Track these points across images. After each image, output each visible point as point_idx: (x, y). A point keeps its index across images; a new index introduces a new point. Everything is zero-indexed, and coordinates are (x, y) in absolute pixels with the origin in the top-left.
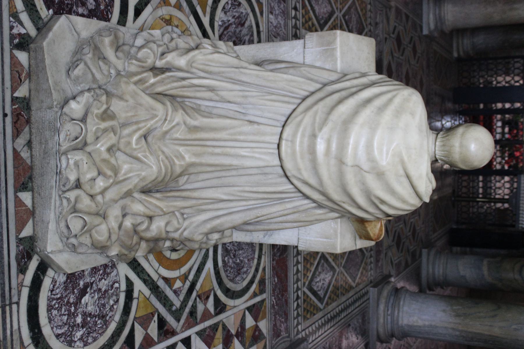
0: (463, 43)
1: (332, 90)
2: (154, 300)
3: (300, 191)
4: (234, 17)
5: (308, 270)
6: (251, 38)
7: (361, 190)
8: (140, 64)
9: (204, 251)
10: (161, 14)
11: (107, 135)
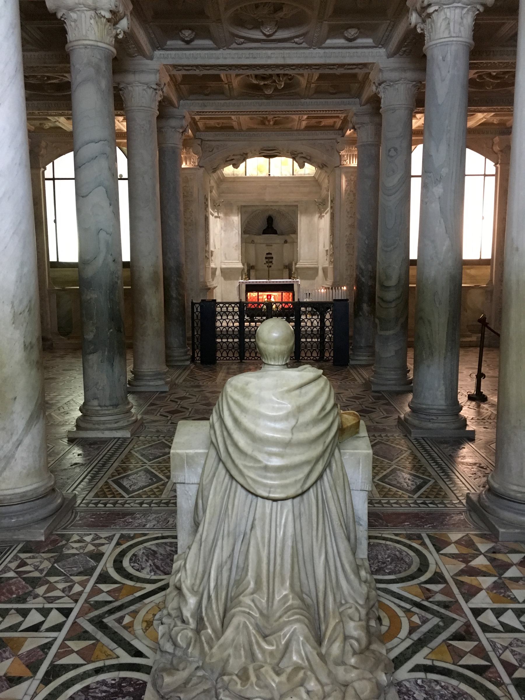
0: (178, 357)
1: (223, 456)
2: (434, 644)
3: (315, 482)
4: (147, 561)
5: (395, 494)
6: (168, 544)
7: (313, 427)
8: (192, 644)
9: (379, 592)
10: (141, 631)
11: (263, 674)
